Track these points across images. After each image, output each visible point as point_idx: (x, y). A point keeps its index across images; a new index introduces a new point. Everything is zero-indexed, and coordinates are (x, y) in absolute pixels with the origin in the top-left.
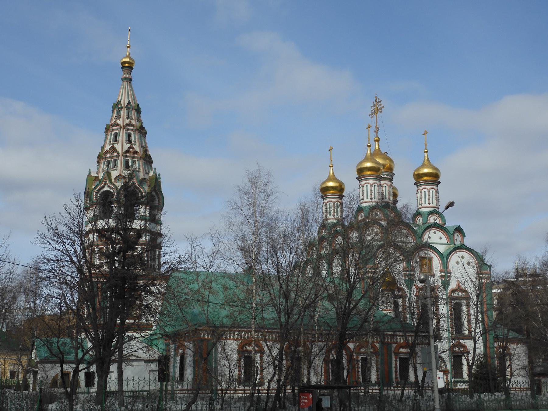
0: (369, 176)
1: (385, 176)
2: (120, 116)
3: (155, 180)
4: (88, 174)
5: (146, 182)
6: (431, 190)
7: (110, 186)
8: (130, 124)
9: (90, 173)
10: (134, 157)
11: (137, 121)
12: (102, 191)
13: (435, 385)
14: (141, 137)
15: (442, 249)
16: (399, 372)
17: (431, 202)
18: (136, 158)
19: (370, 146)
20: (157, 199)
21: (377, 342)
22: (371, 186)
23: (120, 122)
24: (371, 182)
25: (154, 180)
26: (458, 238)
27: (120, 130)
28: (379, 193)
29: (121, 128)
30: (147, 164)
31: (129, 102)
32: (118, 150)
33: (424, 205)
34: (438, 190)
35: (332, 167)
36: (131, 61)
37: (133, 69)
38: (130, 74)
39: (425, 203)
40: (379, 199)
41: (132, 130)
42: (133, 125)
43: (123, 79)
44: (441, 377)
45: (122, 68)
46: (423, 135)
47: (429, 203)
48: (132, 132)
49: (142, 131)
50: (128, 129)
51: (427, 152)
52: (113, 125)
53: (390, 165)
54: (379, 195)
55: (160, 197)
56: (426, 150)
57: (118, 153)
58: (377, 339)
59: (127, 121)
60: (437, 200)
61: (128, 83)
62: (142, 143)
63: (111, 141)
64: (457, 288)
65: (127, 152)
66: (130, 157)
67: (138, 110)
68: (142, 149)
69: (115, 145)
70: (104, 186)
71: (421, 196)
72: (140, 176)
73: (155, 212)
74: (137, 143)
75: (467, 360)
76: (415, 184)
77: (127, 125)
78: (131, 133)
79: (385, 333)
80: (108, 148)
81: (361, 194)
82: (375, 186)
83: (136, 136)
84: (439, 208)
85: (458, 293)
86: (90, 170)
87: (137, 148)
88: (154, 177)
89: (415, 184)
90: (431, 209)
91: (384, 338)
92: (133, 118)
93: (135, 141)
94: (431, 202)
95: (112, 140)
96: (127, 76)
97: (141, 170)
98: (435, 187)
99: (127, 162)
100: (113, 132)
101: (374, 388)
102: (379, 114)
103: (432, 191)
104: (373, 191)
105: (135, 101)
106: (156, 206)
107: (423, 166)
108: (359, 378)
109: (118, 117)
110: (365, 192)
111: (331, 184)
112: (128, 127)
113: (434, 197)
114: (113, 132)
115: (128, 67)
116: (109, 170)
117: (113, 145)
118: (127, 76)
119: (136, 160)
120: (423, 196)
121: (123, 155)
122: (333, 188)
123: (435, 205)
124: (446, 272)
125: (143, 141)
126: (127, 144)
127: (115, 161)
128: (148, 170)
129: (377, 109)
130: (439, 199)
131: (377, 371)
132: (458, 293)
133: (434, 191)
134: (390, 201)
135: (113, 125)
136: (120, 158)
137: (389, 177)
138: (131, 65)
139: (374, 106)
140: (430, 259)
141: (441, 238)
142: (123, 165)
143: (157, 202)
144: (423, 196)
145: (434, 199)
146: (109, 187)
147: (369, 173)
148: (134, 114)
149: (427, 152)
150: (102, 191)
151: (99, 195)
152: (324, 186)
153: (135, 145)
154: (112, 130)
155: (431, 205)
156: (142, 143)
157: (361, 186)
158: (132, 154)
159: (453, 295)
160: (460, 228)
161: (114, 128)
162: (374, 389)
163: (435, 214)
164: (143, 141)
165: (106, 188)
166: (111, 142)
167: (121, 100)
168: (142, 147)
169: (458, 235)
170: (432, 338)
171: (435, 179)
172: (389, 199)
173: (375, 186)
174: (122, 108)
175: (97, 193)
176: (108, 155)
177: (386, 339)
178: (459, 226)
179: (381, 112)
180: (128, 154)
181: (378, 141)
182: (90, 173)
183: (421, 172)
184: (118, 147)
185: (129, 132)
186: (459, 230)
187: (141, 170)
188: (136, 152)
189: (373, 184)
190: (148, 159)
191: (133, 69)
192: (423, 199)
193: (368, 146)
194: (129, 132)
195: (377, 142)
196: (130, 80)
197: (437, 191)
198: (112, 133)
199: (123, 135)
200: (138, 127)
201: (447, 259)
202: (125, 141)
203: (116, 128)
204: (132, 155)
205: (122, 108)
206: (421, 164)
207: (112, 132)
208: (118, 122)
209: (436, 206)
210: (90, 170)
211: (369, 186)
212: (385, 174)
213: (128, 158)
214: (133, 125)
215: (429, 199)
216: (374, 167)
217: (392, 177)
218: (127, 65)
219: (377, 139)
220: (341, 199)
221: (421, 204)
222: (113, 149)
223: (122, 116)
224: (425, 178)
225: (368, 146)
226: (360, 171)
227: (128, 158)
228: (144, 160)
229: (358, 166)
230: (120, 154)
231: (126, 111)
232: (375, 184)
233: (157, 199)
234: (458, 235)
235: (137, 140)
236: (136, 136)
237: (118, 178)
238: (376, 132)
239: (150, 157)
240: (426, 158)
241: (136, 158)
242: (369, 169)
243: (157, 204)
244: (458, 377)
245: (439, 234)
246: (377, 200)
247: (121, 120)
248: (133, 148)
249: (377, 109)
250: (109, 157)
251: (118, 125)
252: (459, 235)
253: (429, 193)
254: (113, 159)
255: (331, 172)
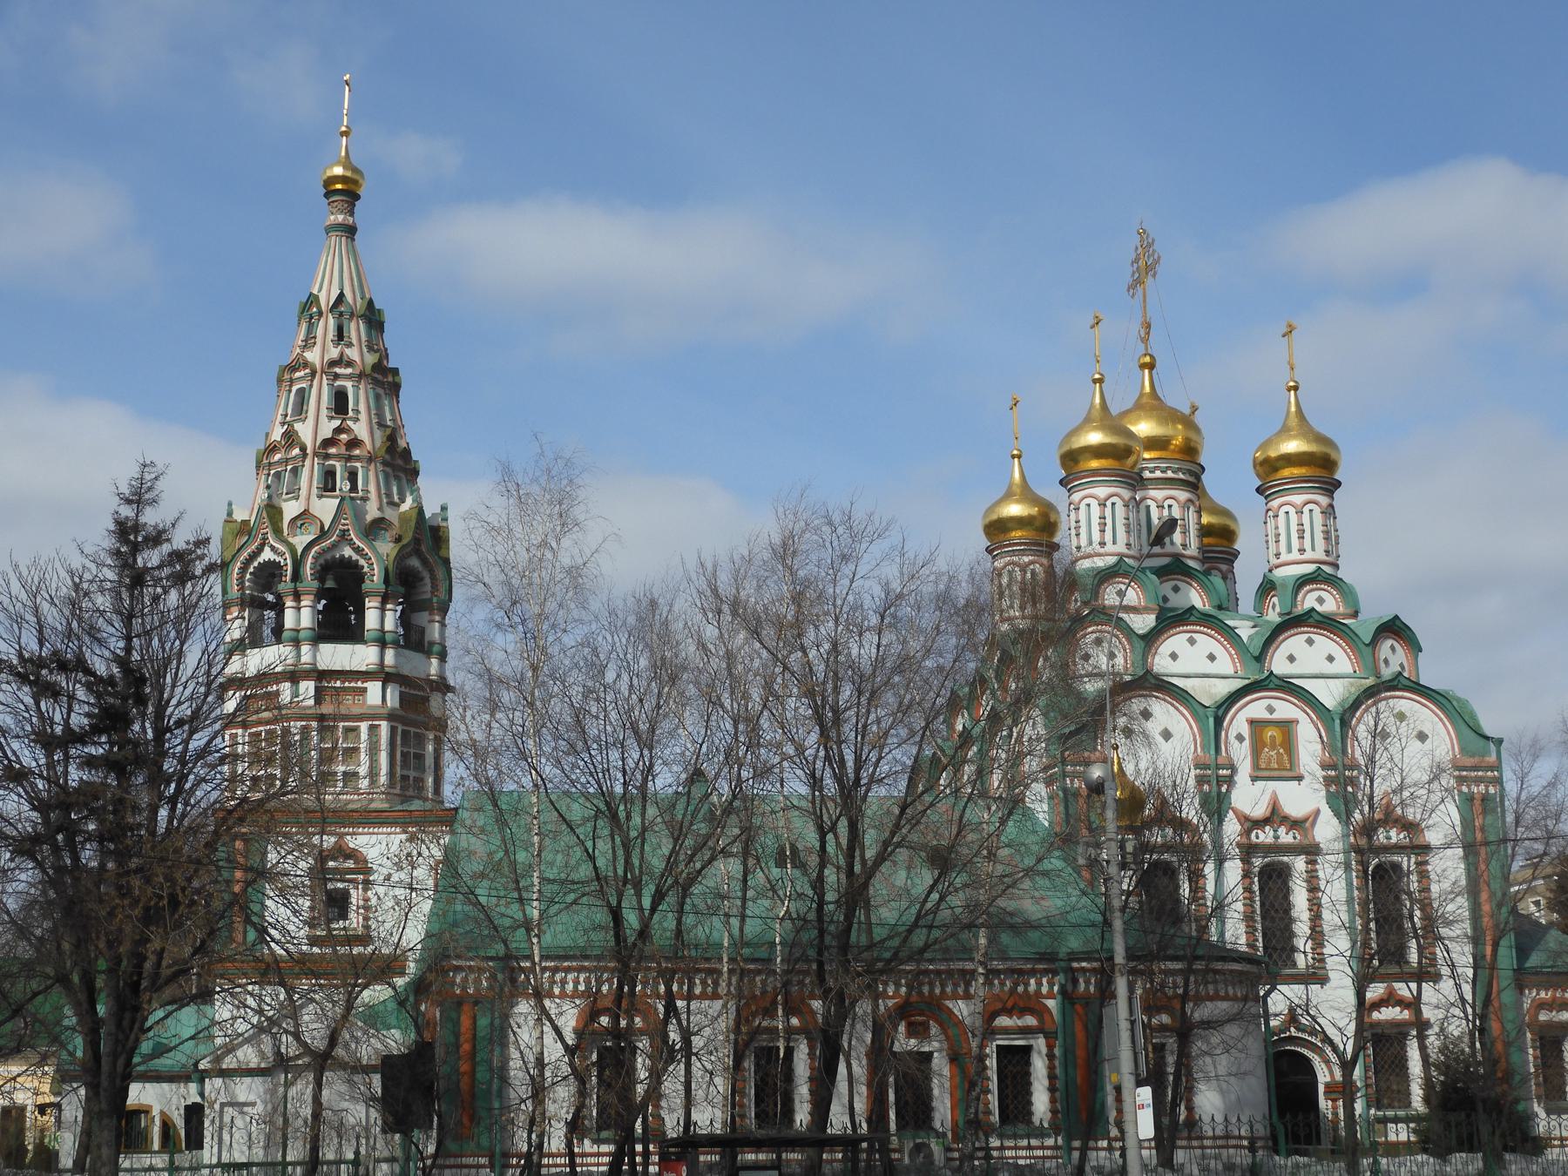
0: (1095, 472)
1: (1158, 474)
2: (315, 337)
3: (417, 523)
4: (225, 516)
5: (386, 530)
6: (1306, 510)
7: (277, 545)
8: (340, 361)
9: (230, 514)
10: (349, 458)
11: (365, 350)
12: (256, 564)
13: (1129, 1128)
14: (378, 398)
15: (1330, 694)
16: (994, 1085)
17: (1307, 545)
18: (358, 458)
19: (1100, 381)
20: (428, 581)
21: (1050, 996)
22: (1103, 505)
23: (313, 356)
24: (1102, 492)
25: (413, 524)
26: (1393, 656)
27: (312, 381)
28: (1127, 526)
29: (313, 373)
30: (397, 478)
31: (341, 296)
32: (303, 438)
33: (1284, 557)
34: (1331, 506)
35: (1019, 457)
36: (349, 174)
37: (357, 197)
38: (352, 214)
39: (1289, 550)
40: (1128, 545)
41: (349, 377)
42: (350, 364)
43: (330, 229)
44: (1145, 1103)
45: (327, 195)
46: (1092, 327)
47: (1302, 551)
48: (349, 385)
49: (384, 380)
50: (337, 376)
51: (1296, 388)
52: (293, 368)
53: (1187, 440)
54: (1128, 532)
55: (440, 573)
56: (1292, 384)
57: (303, 449)
58: (1051, 984)
59: (334, 353)
60: (1327, 538)
61: (344, 239)
62: (380, 415)
63: (286, 415)
64: (1268, 814)
65: (328, 443)
66: (337, 457)
67: (373, 319)
68: (378, 434)
69: (298, 426)
70: (260, 550)
71: (1277, 528)
72: (366, 512)
73: (421, 618)
74: (363, 416)
75: (1423, 1048)
76: (1258, 490)
77: (333, 363)
78: (345, 387)
79: (1075, 965)
80: (277, 434)
81: (1271, 539)
82: (1113, 504)
83: (362, 393)
84: (1336, 566)
85: (1275, 831)
86: (230, 504)
87: (361, 429)
88: (414, 514)
89: (1258, 490)
90: (1310, 568)
91: (1075, 982)
92: (354, 341)
93: (357, 412)
94: (1307, 545)
95: (289, 411)
96: (340, 218)
97: (373, 495)
98: (1324, 500)
99: (329, 475)
100: (294, 389)
101: (1050, 1142)
102: (1149, 281)
103: (1311, 511)
104: (1109, 521)
105: (362, 292)
106: (424, 601)
107: (1284, 432)
108: (988, 1112)
109: (309, 342)
110: (1083, 523)
111: (1015, 509)
112: (337, 370)
113: (1319, 529)
114: (294, 389)
115: (346, 193)
116: (275, 501)
117: (290, 425)
118: (340, 218)
119: (358, 465)
120: (1282, 530)
121: (315, 454)
122: (1020, 522)
123: (1320, 554)
124: (1213, 765)
125: (387, 409)
126: (331, 418)
127: (295, 471)
128: (399, 494)
129: (1145, 267)
130: (1337, 537)
131: (1052, 1089)
132: (1275, 831)
133: (1317, 510)
134: (1187, 553)
135: (293, 368)
136: (308, 462)
137: (1181, 476)
138: (352, 187)
139: (1136, 261)
140: (1287, 726)
141: (1212, 658)
142: (315, 484)
143: (428, 588)
144: (1282, 530)
145: (1319, 536)
146: (273, 548)
147: (1094, 464)
148: (356, 330)
149: (1296, 388)
150: (256, 564)
151: (248, 576)
152: (994, 517)
153: (357, 420)
154: (292, 382)
155: (1309, 555)
156: (380, 415)
157: (1270, 513)
158: (344, 448)
159: (1257, 837)
160: (1397, 623)
161: (298, 374)
162: (1022, 1148)
163: (1321, 582)
164: (387, 409)
165: (267, 555)
166: (288, 418)
167: (320, 290)
168: (381, 425)
169: (1393, 648)
170: (1122, 975)
171: (1318, 472)
172: (1184, 546)
173: (1113, 504)
174: (320, 314)
175: (244, 569)
176: (277, 457)
177: (1082, 986)
178: (1396, 617)
179: (1154, 276)
180: (333, 451)
181: (1151, 366)
182: (230, 514)
183: (1273, 454)
184: (305, 431)
185: (338, 383)
186: (1394, 629)
187: (373, 495)
188: (355, 443)
189: (1106, 500)
190: (400, 462)
191: (357, 197)
192: (1283, 538)
193: (1095, 381)
194: (338, 383)
195: (1147, 371)
196: (350, 231)
197: (1329, 512)
198: (290, 391)
199: (320, 396)
200: (368, 370)
201: (1219, 722)
202: (324, 412)
203: (302, 373)
204: (343, 450)
205: (320, 314)
206: (1279, 428)
207: (291, 386)
208: (308, 355)
209: (1323, 557)
210: (230, 504)
211: (1094, 503)
212: (1156, 468)
213: (331, 462)
214: (350, 364)
215: (1301, 537)
216: (1304, 453)
217: (1198, 478)
218: (339, 186)
219: (1147, 359)
220: (1049, 555)
221: (1278, 555)
222: (290, 437)
223: (319, 340)
224: (1286, 472)
225: (1095, 381)
226: (1071, 458)
227: (331, 462)
228: (385, 463)
229: (1061, 446)
230: (309, 451)
231: (331, 321)
232: (1114, 499)
233: (428, 581)
234: (1393, 648)
235: (362, 407)
236: (362, 393)
237: (299, 523)
238: (1145, 340)
239: (406, 453)
240: (1293, 409)
241: (358, 458)
242: (1098, 451)
243: (428, 596)
244: (1396, 1104)
245: (1325, 644)
246: (1121, 547)
247: (317, 349)
248: (348, 430)
249: (1145, 267)
250: (279, 462)
251: (306, 364)
252: (1396, 644)
253: (1300, 518)
254: (289, 468)
255: (1017, 475)
